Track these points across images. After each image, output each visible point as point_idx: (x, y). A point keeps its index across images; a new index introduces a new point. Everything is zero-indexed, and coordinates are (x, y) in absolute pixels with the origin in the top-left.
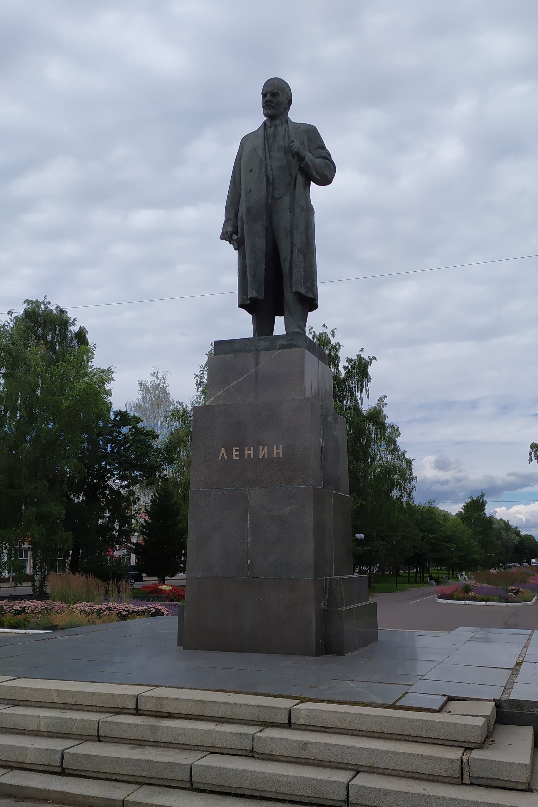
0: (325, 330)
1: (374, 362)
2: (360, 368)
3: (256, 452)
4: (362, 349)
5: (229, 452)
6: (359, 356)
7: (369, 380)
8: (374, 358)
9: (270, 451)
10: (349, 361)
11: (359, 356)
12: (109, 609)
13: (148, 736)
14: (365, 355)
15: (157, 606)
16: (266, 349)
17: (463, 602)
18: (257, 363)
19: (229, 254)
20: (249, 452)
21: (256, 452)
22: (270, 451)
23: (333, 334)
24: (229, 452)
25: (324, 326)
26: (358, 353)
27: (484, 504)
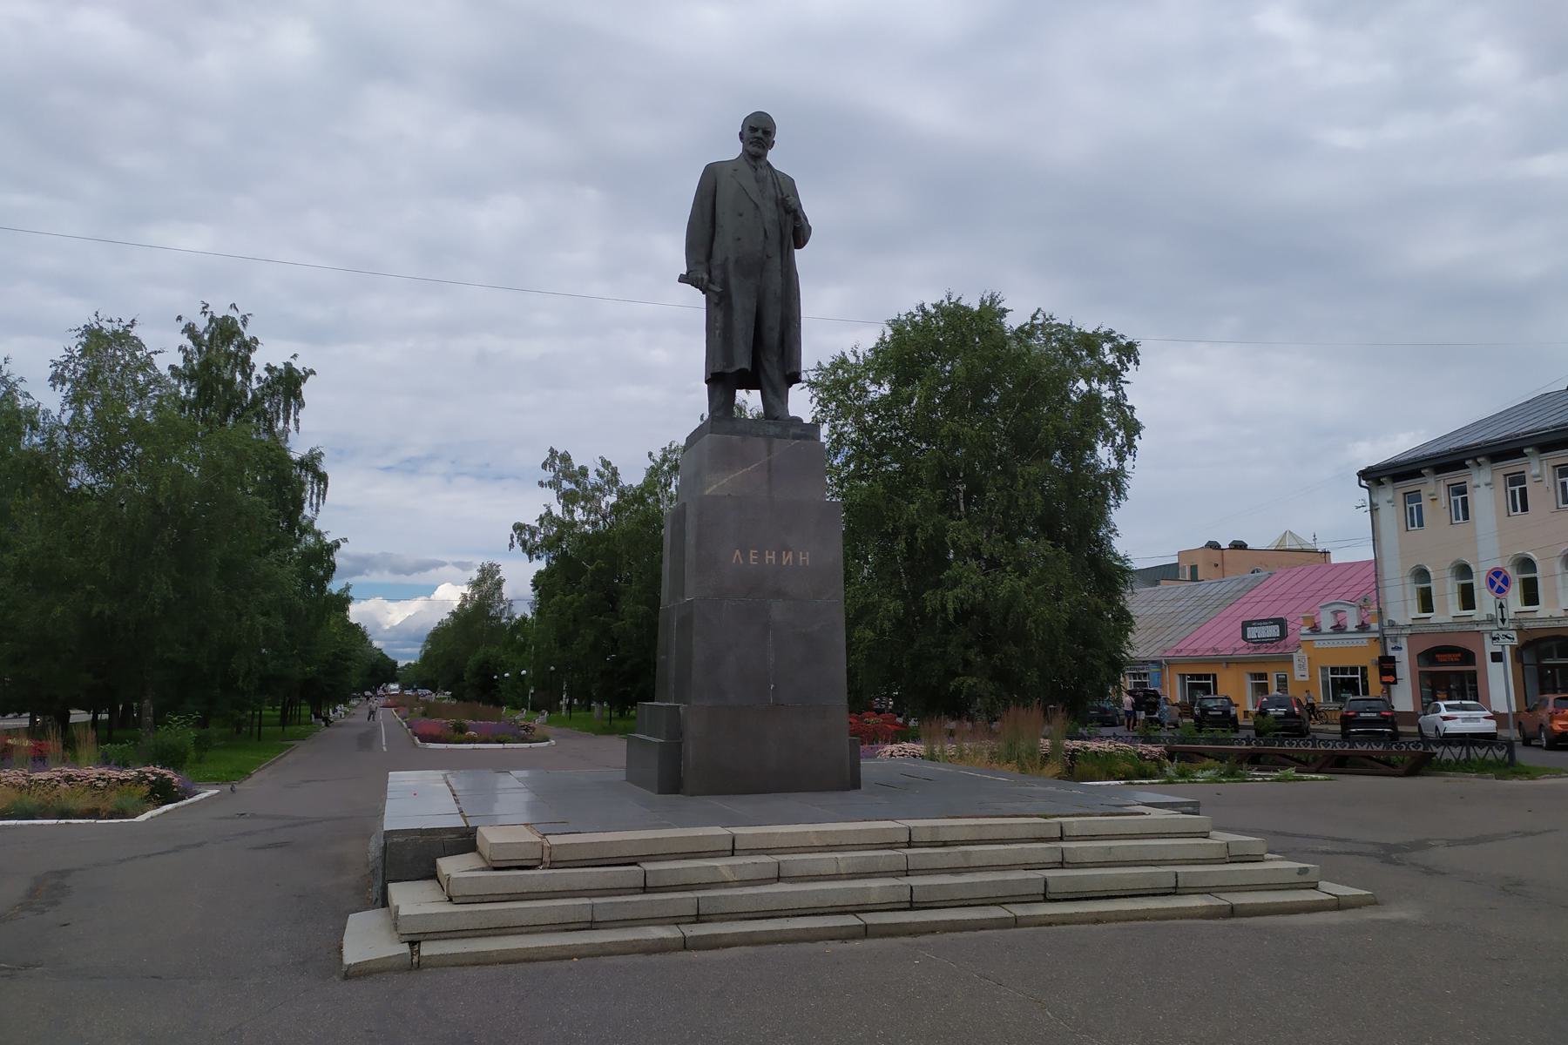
0: (233, 313)
1: (311, 377)
2: (288, 384)
3: (779, 556)
4: (295, 356)
5: (745, 556)
6: (288, 365)
7: (301, 405)
8: (312, 372)
9: (795, 559)
10: (269, 369)
11: (288, 365)
12: (68, 779)
13: (962, 863)
14: (297, 365)
15: (158, 770)
16: (778, 437)
17: (471, 746)
18: (770, 452)
19: (696, 301)
20: (770, 557)
21: (779, 556)
22: (795, 559)
23: (245, 320)
24: (745, 556)
25: (233, 306)
26: (288, 359)
27: (348, 600)
